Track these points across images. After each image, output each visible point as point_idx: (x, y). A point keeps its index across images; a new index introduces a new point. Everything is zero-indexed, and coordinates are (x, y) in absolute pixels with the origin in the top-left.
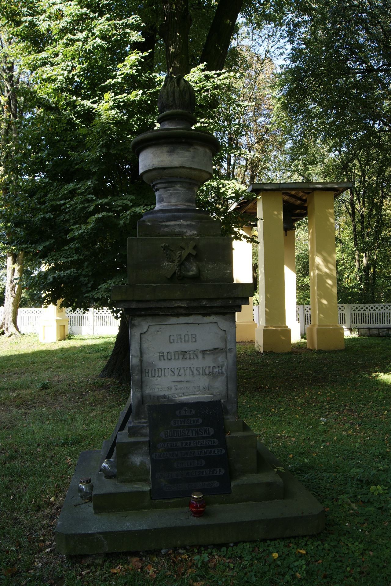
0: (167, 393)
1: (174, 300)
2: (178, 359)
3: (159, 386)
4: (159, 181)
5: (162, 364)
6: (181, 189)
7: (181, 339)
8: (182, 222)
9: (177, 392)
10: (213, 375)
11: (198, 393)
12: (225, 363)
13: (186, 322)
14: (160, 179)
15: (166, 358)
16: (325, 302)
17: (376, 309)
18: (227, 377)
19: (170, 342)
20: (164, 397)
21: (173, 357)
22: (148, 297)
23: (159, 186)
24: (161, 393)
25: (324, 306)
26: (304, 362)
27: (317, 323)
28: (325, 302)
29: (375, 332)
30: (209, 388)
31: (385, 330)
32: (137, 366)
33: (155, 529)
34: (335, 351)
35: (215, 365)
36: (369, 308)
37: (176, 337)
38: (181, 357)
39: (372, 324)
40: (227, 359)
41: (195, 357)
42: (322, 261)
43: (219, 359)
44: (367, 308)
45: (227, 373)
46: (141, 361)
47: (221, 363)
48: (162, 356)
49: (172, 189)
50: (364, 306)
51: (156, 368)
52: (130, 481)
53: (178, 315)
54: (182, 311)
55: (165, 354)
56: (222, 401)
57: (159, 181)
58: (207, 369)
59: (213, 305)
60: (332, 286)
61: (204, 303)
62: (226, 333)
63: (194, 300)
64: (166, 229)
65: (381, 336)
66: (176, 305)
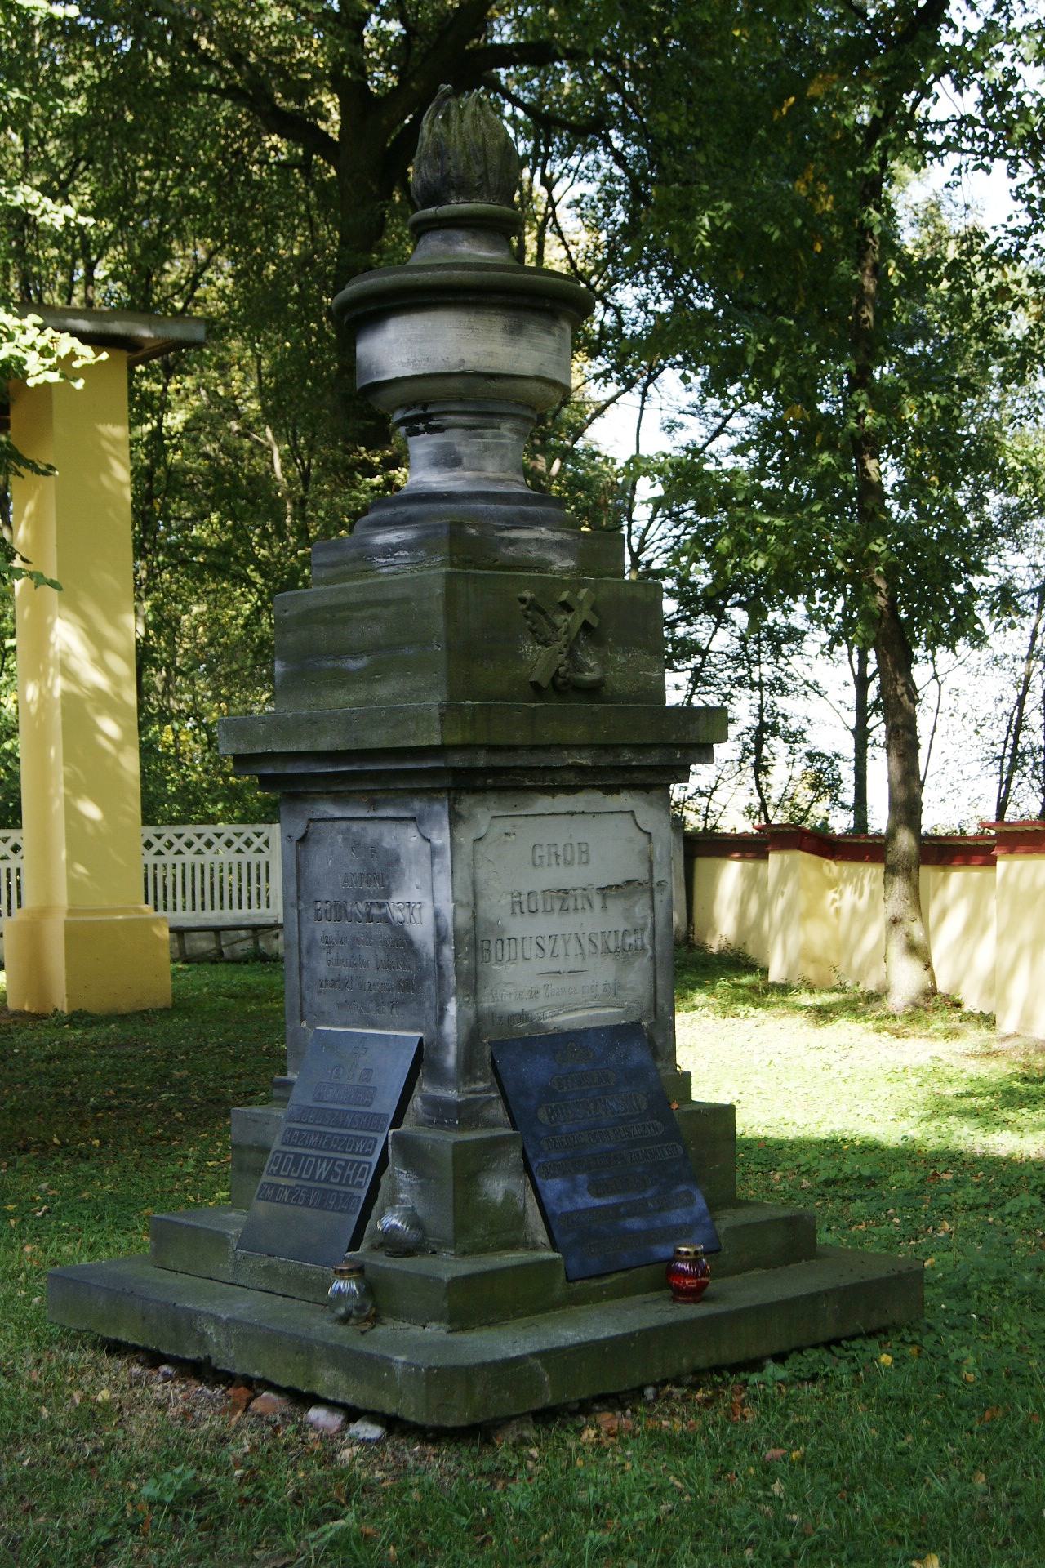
0: (527, 1006)
1: (568, 747)
2: (552, 910)
3: (511, 988)
4: (457, 408)
5: (517, 927)
6: (509, 435)
7: (557, 856)
8: (542, 532)
9: (550, 1001)
10: (624, 954)
11: (593, 1003)
12: (649, 921)
13: (571, 809)
14: (461, 401)
15: (525, 909)
16: (91, 810)
17: (204, 849)
18: (653, 958)
19: (535, 865)
20: (522, 1017)
21: (541, 908)
22: (519, 738)
23: (451, 419)
24: (516, 1008)
25: (89, 829)
26: (62, 1057)
27: (62, 899)
28: (91, 810)
29: (203, 944)
30: (618, 987)
31: (243, 933)
32: (468, 932)
33: (640, 1331)
34: (144, 1016)
35: (628, 927)
36: (179, 844)
37: (545, 849)
38: (557, 906)
39: (189, 913)
40: (653, 908)
41: (587, 906)
42: (82, 640)
43: (637, 910)
44: (170, 845)
45: (654, 949)
46: (475, 918)
47: (641, 922)
48: (520, 904)
49: (489, 432)
50: (180, 836)
51: (505, 937)
52: (482, 1250)
53: (551, 790)
54: (571, 778)
55: (524, 898)
56: (645, 1023)
57: (457, 408)
58: (613, 936)
59: (644, 763)
60: (119, 745)
61: (627, 755)
62: (650, 841)
63: (605, 748)
64: (510, 551)
65: (228, 962)
66: (570, 761)
